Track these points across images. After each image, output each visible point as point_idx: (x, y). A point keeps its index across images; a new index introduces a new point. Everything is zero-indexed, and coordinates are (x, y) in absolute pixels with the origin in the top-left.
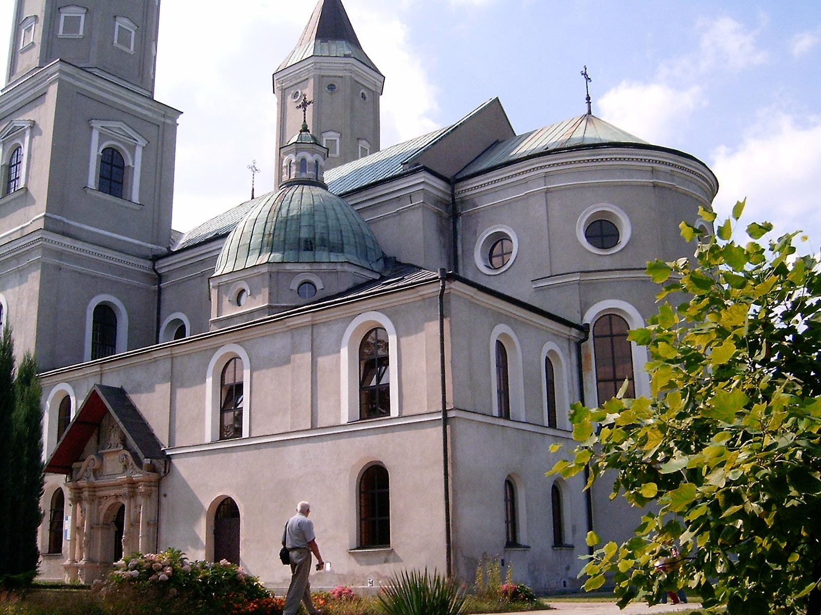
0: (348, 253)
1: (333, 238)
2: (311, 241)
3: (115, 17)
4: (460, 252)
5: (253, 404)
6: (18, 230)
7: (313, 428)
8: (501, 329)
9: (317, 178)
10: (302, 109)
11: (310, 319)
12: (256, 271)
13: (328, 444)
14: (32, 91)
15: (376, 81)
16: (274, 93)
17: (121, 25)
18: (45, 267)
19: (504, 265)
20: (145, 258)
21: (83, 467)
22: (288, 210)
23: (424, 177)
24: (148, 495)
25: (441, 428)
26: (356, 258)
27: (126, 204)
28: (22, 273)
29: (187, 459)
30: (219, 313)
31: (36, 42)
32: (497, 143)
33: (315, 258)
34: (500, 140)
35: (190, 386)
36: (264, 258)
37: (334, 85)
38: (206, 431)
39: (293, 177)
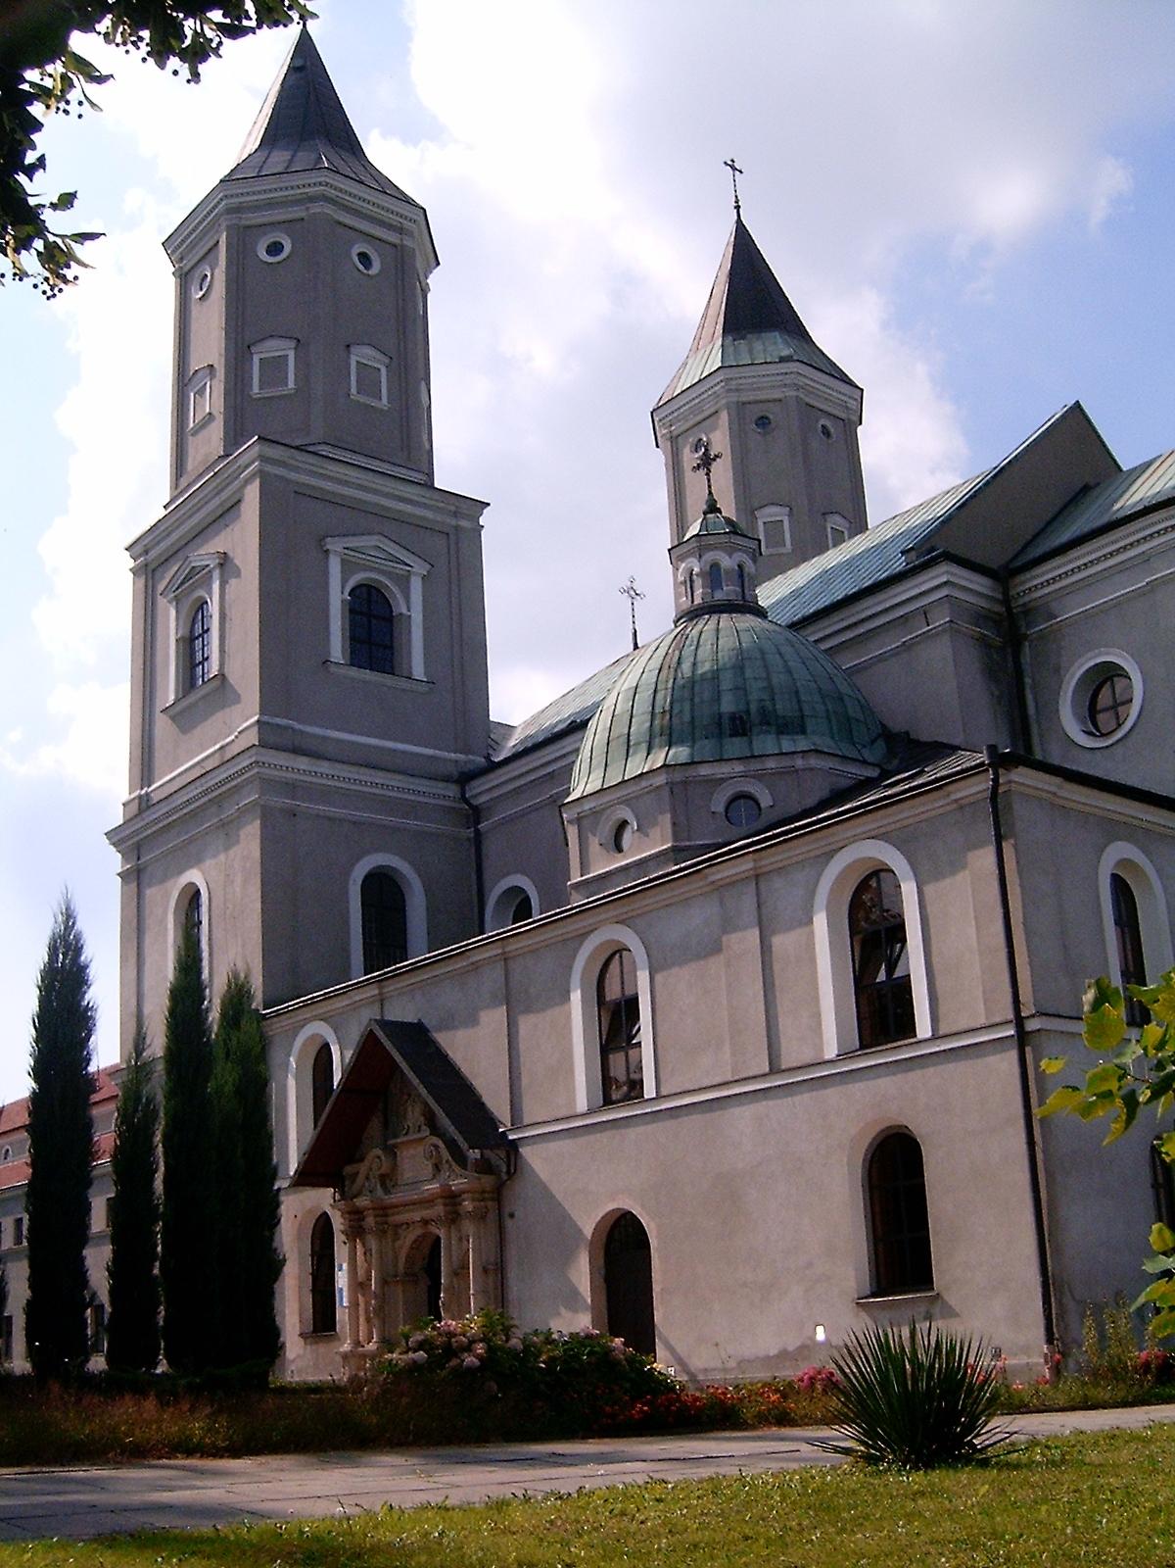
0: (814, 732)
1: (784, 707)
2: (741, 718)
3: (348, 346)
4: (1031, 710)
5: (660, 1034)
6: (215, 752)
7: (774, 1070)
8: (1119, 851)
9: (743, 598)
10: (702, 472)
11: (751, 865)
12: (644, 784)
13: (805, 1098)
14: (216, 501)
15: (845, 399)
16: (657, 446)
17: (358, 359)
18: (267, 816)
19: (1120, 725)
20: (447, 779)
21: (361, 1171)
22: (694, 664)
23: (947, 572)
24: (480, 1217)
25: (1014, 1054)
26: (828, 740)
27: (403, 683)
28: (228, 829)
29: (545, 1145)
30: (584, 868)
31: (215, 413)
32: (1086, 489)
33: (751, 749)
34: (1092, 484)
35: (543, 1010)
36: (658, 759)
37: (767, 418)
38: (577, 1092)
39: (698, 601)
